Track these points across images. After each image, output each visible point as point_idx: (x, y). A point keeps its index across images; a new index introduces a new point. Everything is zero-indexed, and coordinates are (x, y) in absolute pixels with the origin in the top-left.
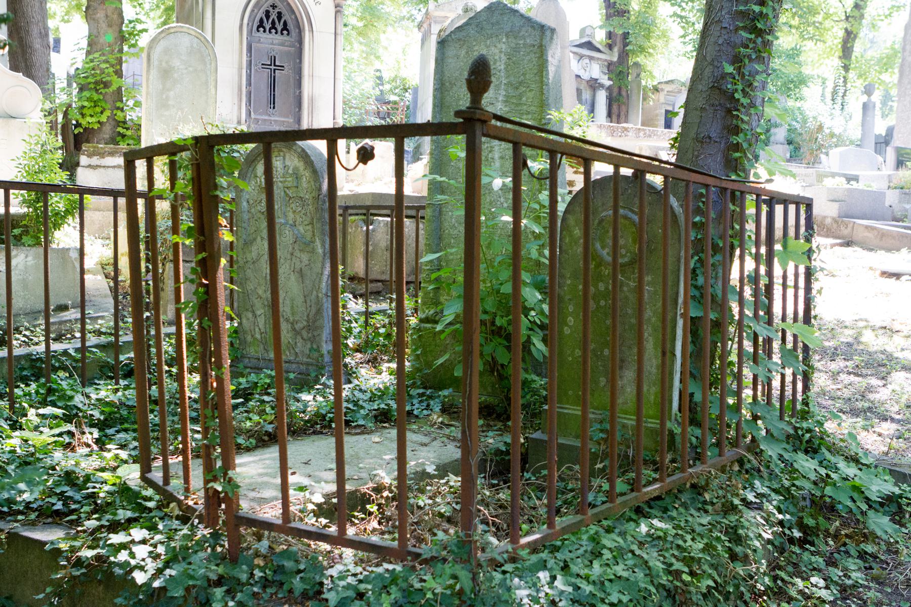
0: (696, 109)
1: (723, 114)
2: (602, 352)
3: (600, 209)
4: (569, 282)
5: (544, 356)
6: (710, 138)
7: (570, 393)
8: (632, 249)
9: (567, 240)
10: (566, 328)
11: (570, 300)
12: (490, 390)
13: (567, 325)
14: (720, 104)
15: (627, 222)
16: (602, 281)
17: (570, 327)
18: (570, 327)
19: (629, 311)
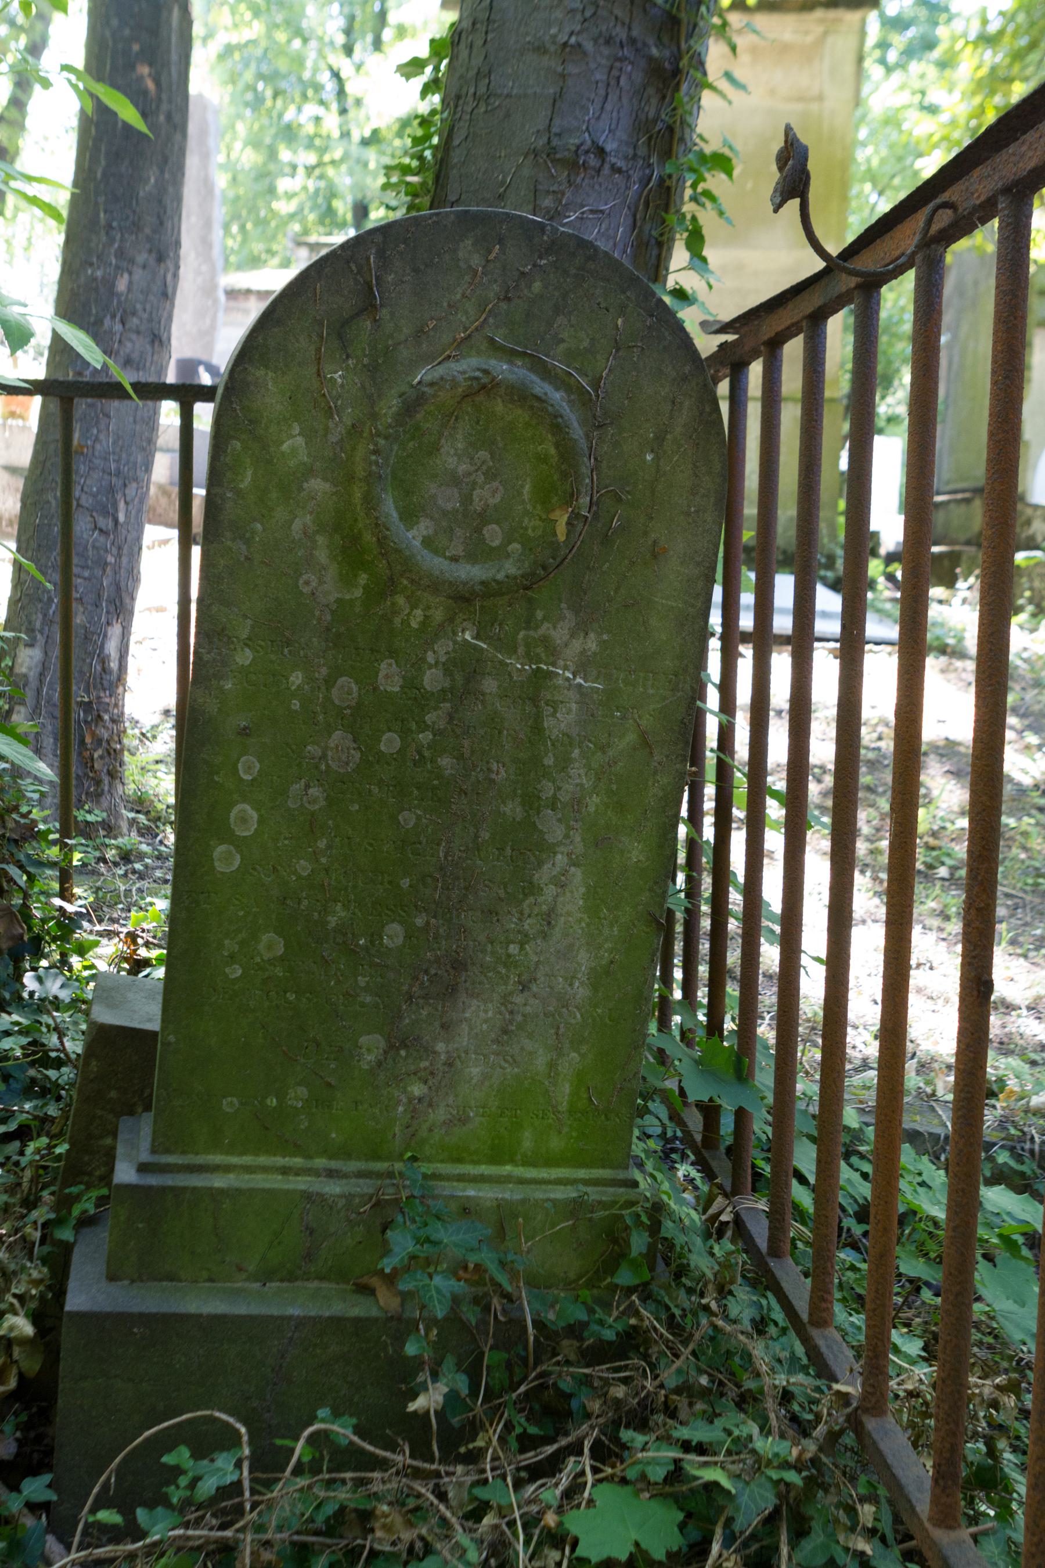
0: (540, 49)
1: (638, 77)
2: (375, 936)
3: (404, 353)
4: (244, 657)
5: (866, 1199)
6: (601, 152)
7: (229, 1104)
8: (533, 527)
9: (247, 480)
10: (220, 849)
11: (244, 732)
12: (455, 1421)
13: (226, 835)
14: (633, 41)
15: (520, 415)
16: (393, 653)
17: (239, 844)
18: (239, 844)
19: (501, 774)
